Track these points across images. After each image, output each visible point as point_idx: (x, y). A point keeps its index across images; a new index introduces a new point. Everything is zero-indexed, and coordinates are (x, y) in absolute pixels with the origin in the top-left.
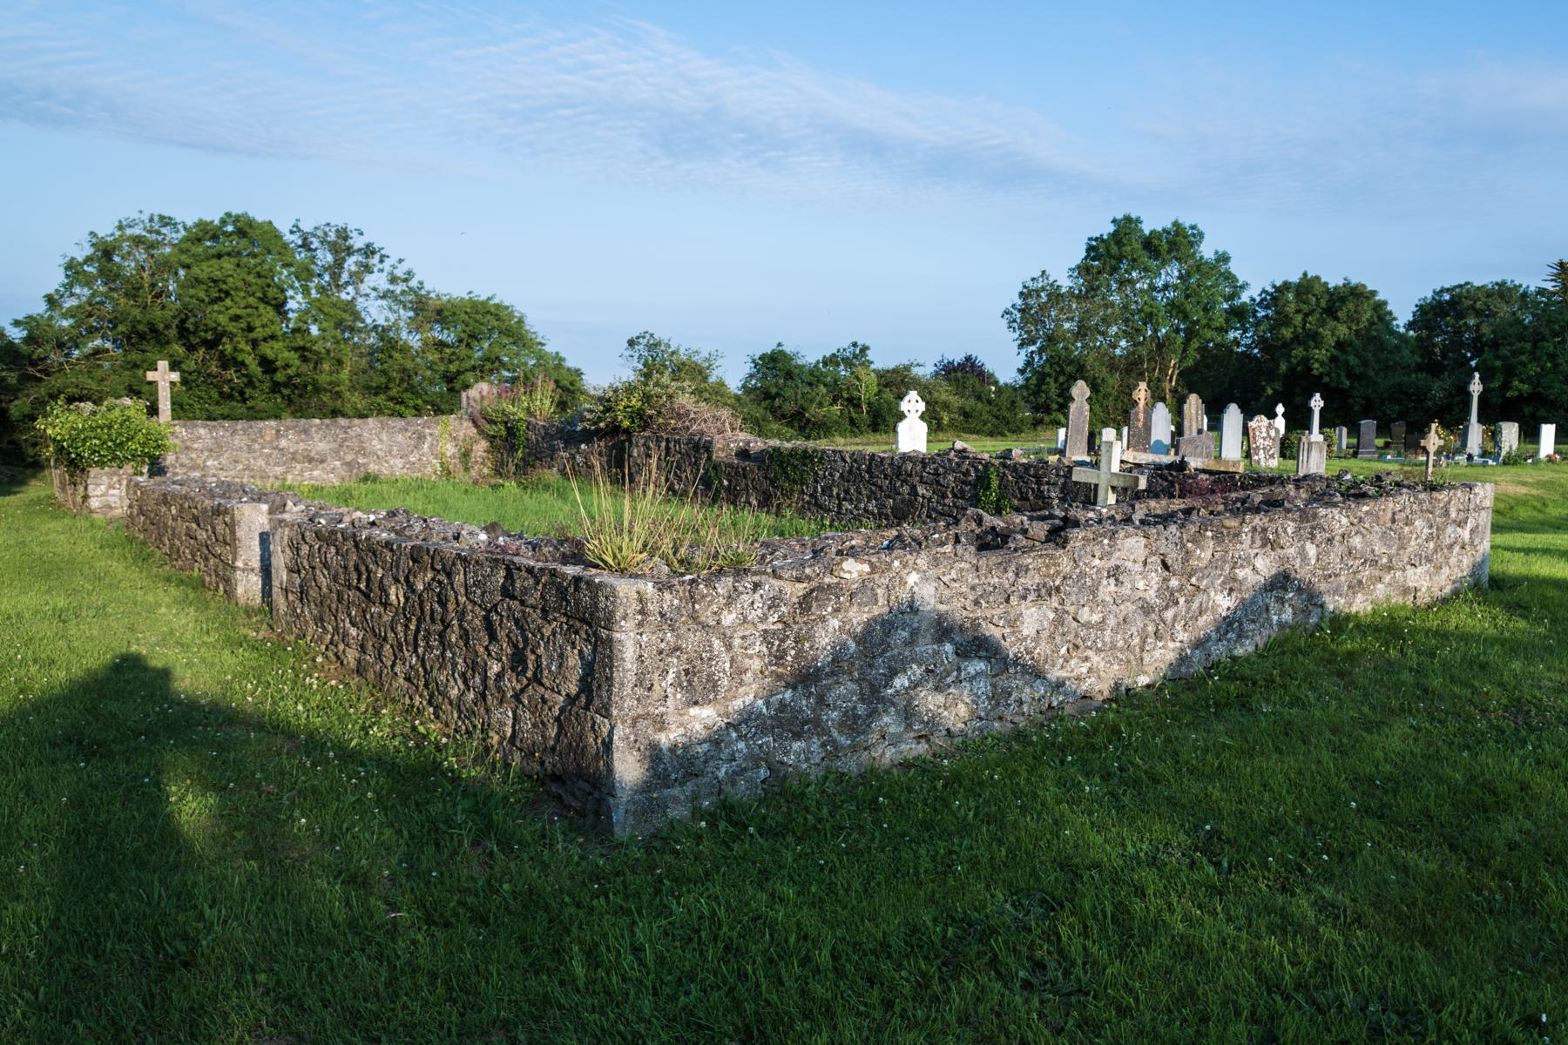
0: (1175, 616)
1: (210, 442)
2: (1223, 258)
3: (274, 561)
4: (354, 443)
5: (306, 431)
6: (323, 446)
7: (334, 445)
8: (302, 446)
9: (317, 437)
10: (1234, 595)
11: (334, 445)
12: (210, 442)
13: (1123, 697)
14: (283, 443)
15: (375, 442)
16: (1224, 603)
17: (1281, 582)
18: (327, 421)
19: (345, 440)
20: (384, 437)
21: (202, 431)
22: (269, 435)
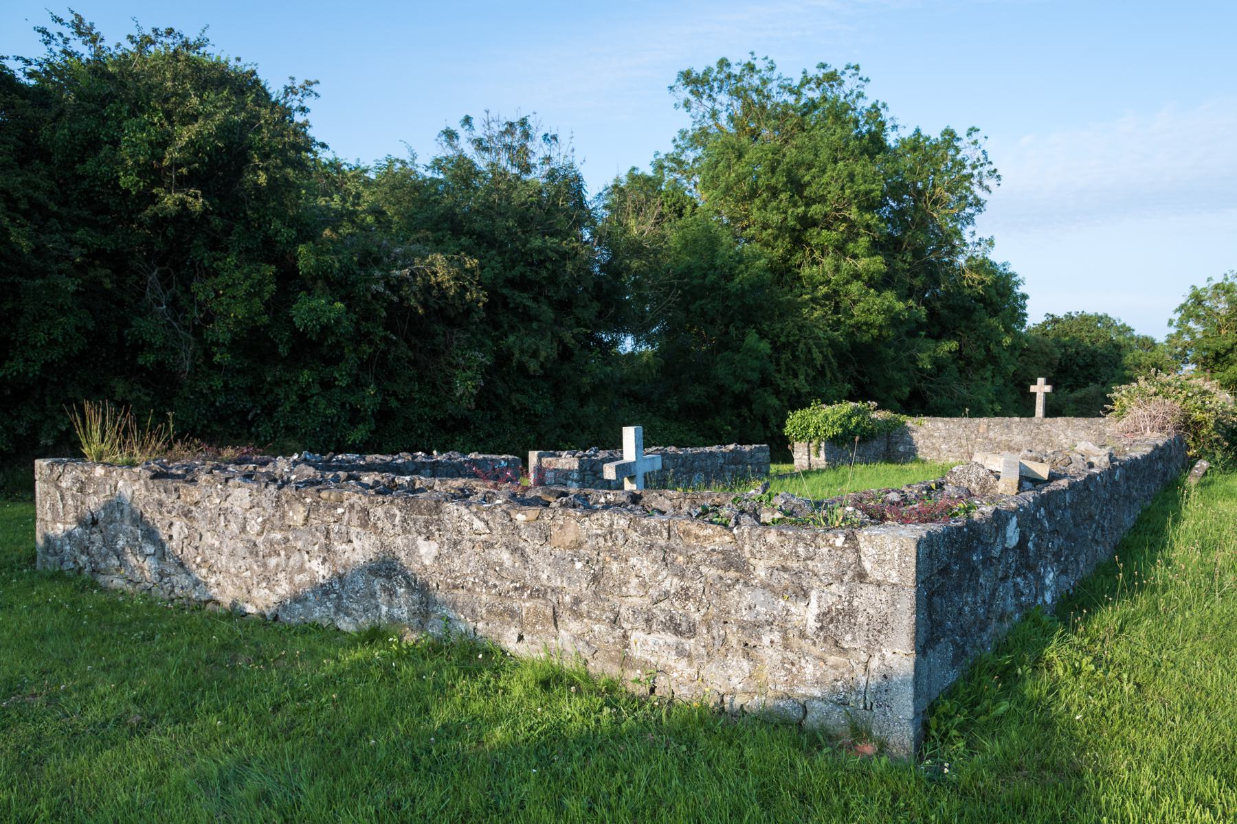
0: (277, 565)
1: (944, 433)
2: (1025, 297)
3: (170, 481)
4: (1045, 437)
5: (1008, 427)
6: (1018, 439)
7: (1028, 438)
8: (1004, 438)
9: (1016, 431)
10: (327, 564)
11: (1028, 438)
12: (944, 433)
13: (235, 613)
14: (991, 435)
15: (1062, 436)
16: (321, 571)
17: (386, 568)
18: (1025, 419)
19: (1037, 434)
20: (1069, 433)
21: (940, 425)
22: (983, 428)
